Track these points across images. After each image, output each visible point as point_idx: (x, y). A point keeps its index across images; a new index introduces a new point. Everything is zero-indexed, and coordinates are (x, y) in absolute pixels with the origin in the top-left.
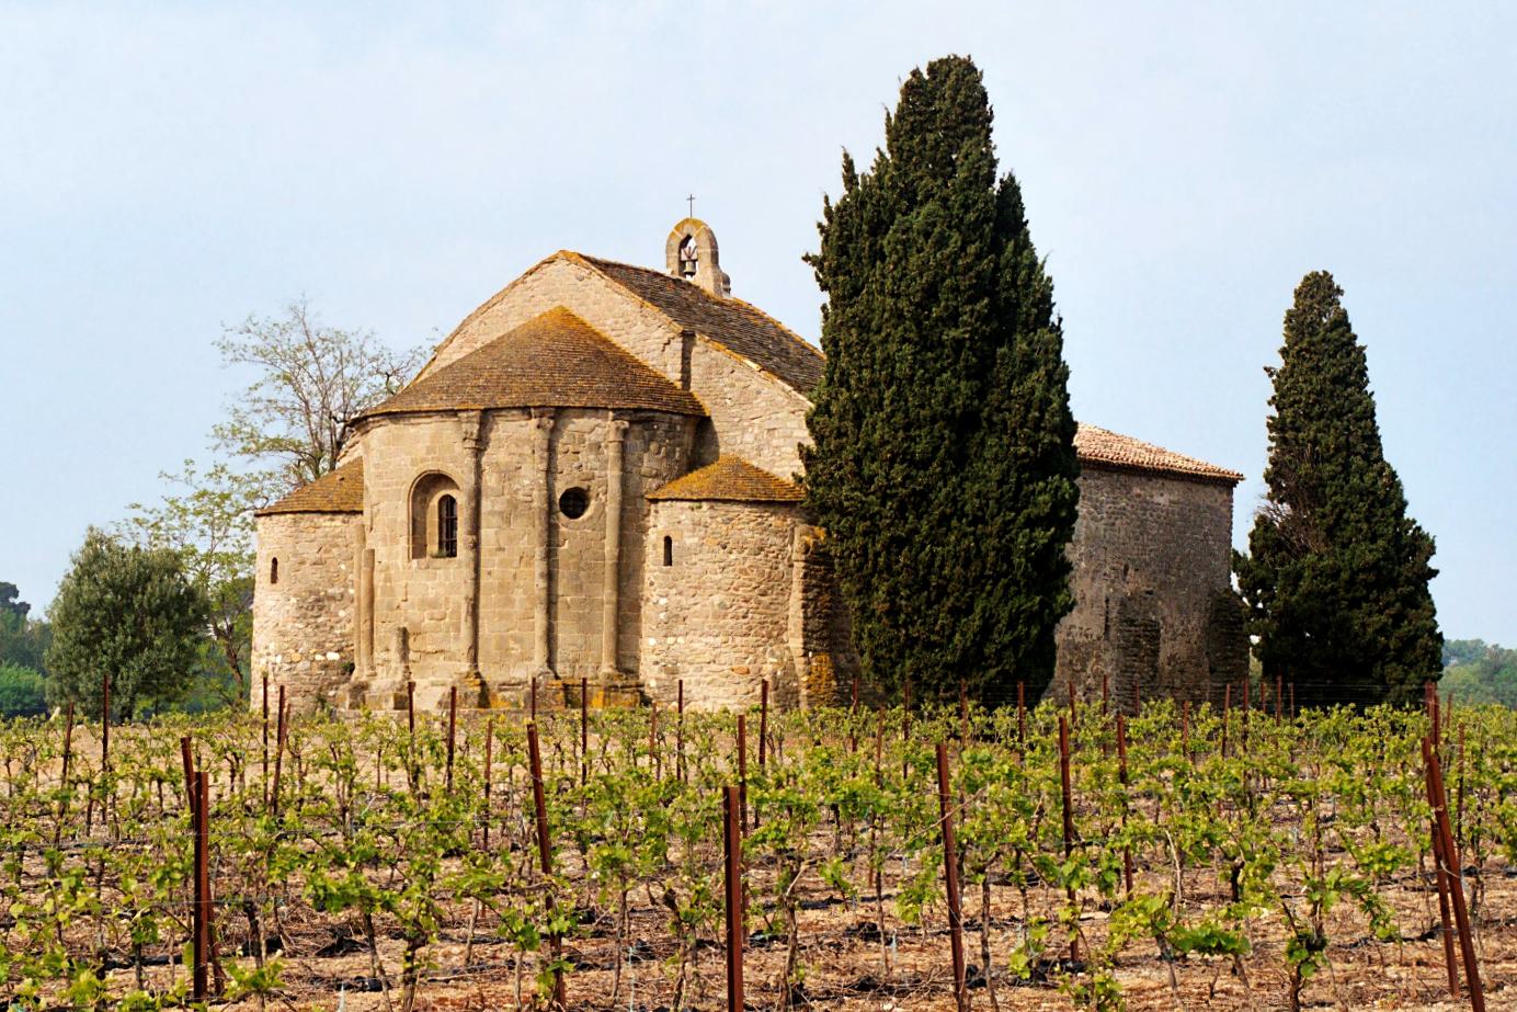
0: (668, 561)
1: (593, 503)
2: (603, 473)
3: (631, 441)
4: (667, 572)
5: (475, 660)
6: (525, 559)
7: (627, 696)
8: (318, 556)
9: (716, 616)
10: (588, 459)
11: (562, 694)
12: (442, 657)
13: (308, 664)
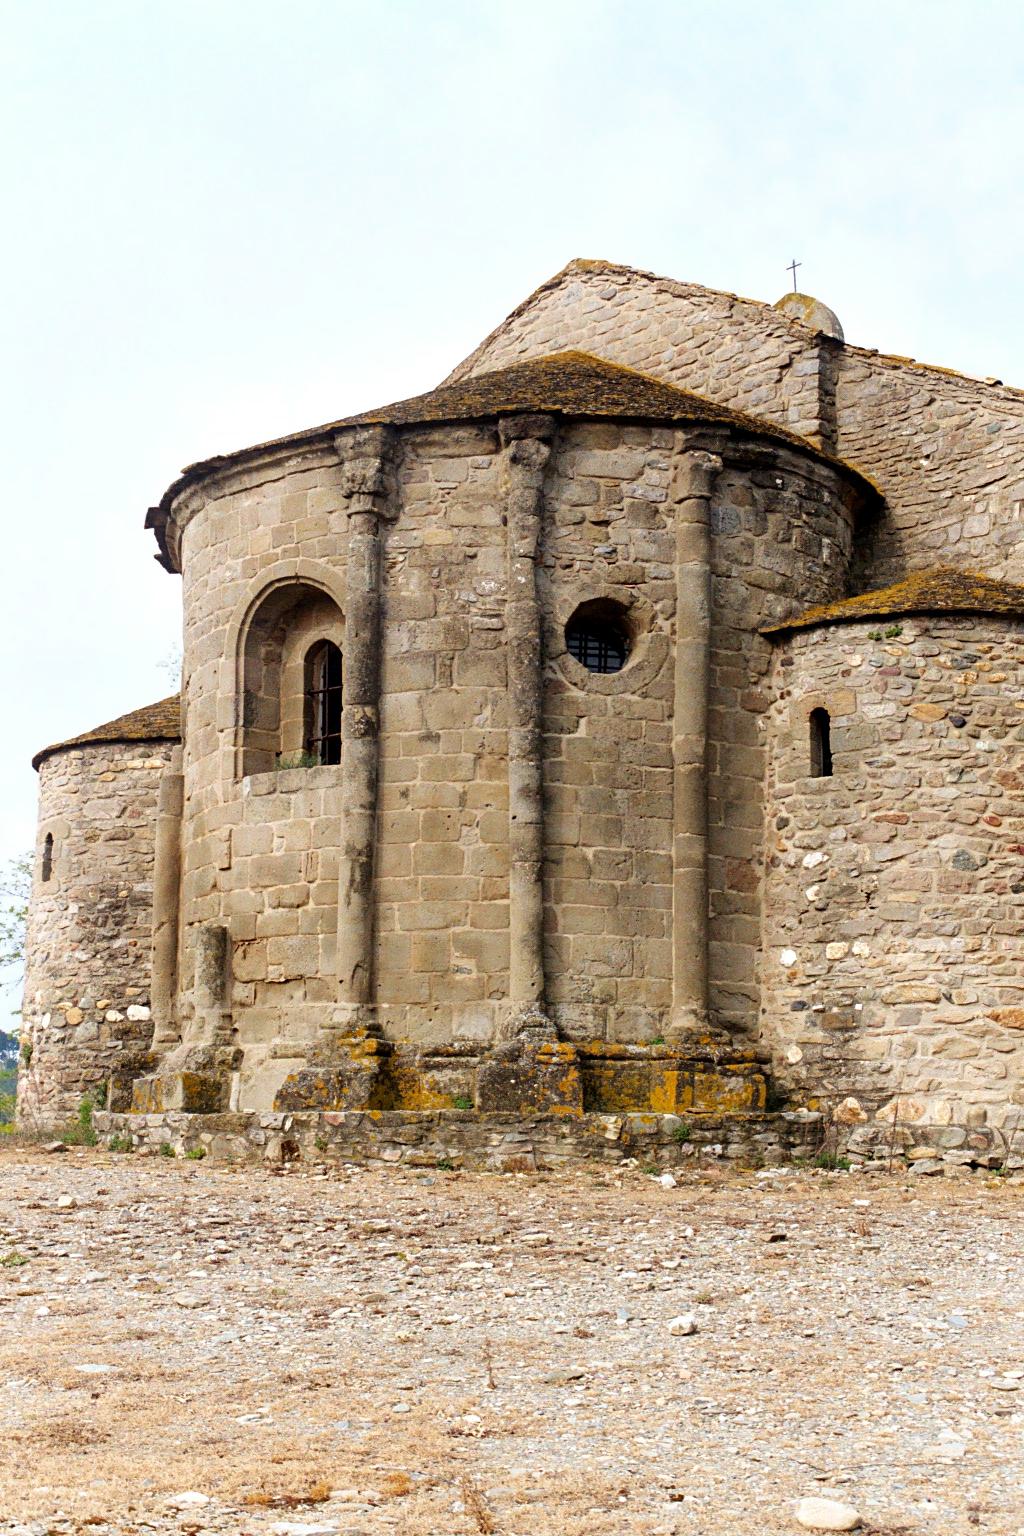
0: (824, 764)
1: (644, 637)
2: (664, 570)
3: (725, 506)
4: (819, 791)
5: (368, 995)
6: (488, 759)
7: (734, 1082)
8: (120, 822)
9: (949, 887)
10: (628, 535)
11: (574, 1074)
12: (299, 994)
13: (92, 1028)
